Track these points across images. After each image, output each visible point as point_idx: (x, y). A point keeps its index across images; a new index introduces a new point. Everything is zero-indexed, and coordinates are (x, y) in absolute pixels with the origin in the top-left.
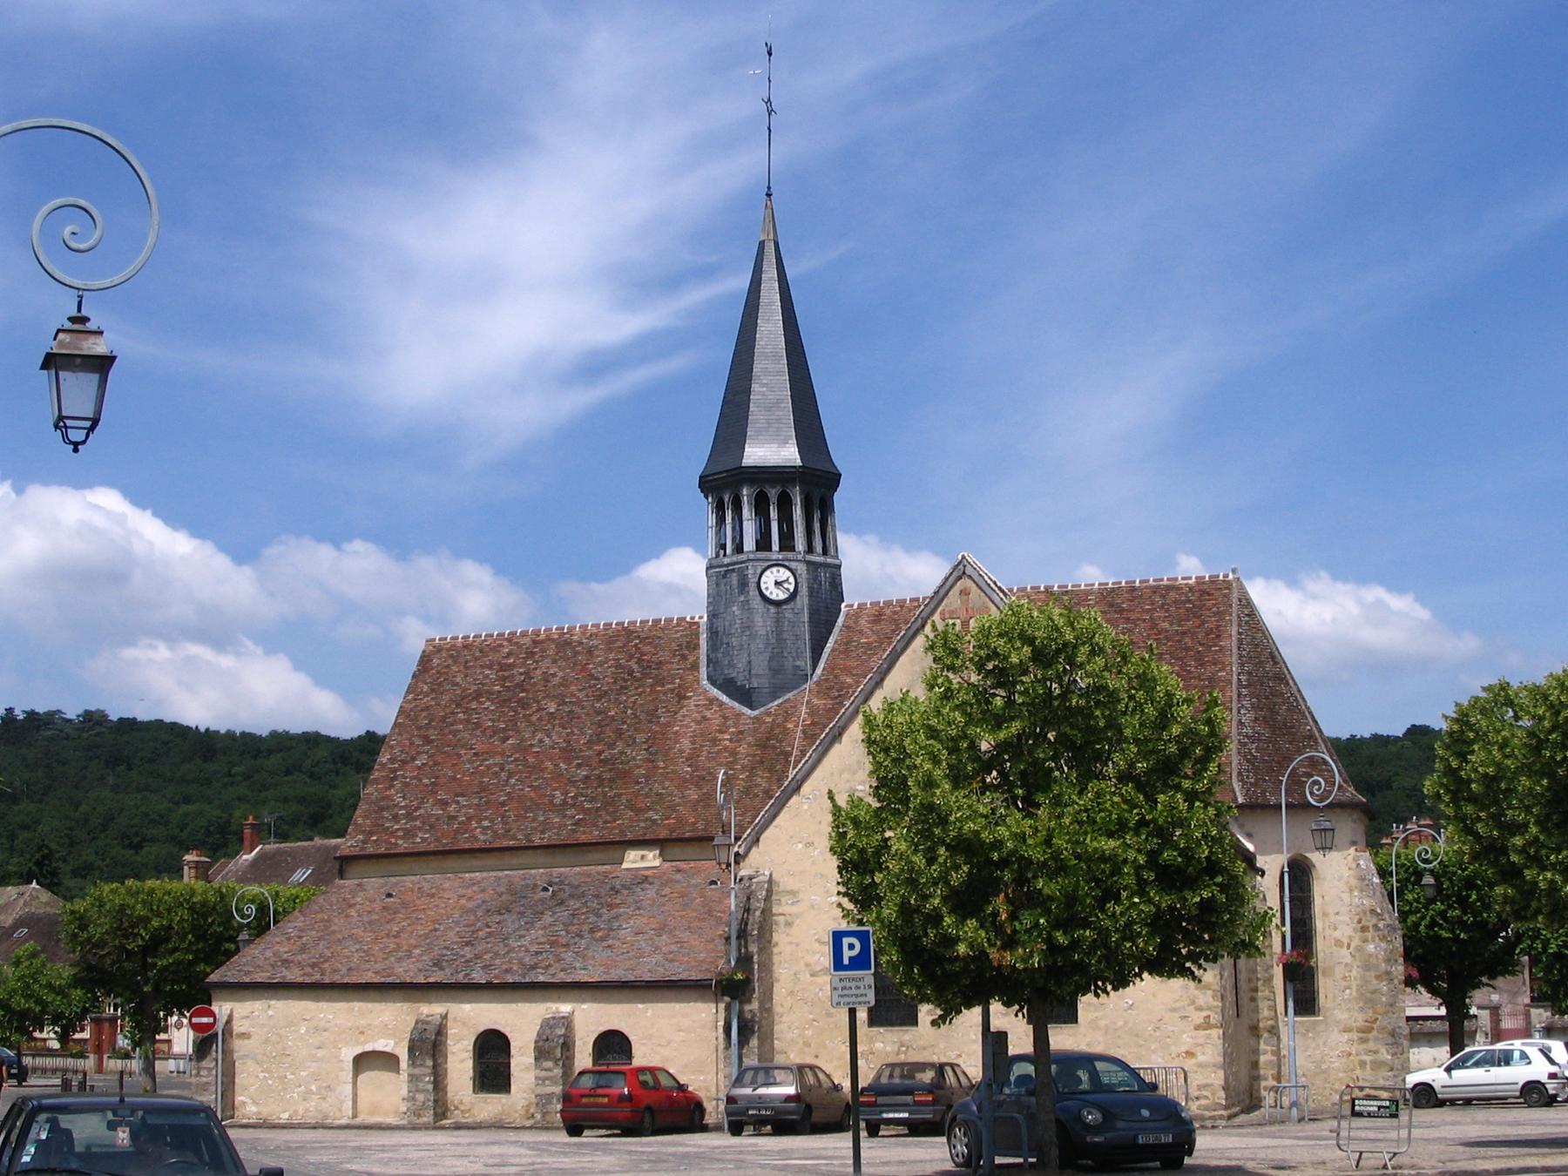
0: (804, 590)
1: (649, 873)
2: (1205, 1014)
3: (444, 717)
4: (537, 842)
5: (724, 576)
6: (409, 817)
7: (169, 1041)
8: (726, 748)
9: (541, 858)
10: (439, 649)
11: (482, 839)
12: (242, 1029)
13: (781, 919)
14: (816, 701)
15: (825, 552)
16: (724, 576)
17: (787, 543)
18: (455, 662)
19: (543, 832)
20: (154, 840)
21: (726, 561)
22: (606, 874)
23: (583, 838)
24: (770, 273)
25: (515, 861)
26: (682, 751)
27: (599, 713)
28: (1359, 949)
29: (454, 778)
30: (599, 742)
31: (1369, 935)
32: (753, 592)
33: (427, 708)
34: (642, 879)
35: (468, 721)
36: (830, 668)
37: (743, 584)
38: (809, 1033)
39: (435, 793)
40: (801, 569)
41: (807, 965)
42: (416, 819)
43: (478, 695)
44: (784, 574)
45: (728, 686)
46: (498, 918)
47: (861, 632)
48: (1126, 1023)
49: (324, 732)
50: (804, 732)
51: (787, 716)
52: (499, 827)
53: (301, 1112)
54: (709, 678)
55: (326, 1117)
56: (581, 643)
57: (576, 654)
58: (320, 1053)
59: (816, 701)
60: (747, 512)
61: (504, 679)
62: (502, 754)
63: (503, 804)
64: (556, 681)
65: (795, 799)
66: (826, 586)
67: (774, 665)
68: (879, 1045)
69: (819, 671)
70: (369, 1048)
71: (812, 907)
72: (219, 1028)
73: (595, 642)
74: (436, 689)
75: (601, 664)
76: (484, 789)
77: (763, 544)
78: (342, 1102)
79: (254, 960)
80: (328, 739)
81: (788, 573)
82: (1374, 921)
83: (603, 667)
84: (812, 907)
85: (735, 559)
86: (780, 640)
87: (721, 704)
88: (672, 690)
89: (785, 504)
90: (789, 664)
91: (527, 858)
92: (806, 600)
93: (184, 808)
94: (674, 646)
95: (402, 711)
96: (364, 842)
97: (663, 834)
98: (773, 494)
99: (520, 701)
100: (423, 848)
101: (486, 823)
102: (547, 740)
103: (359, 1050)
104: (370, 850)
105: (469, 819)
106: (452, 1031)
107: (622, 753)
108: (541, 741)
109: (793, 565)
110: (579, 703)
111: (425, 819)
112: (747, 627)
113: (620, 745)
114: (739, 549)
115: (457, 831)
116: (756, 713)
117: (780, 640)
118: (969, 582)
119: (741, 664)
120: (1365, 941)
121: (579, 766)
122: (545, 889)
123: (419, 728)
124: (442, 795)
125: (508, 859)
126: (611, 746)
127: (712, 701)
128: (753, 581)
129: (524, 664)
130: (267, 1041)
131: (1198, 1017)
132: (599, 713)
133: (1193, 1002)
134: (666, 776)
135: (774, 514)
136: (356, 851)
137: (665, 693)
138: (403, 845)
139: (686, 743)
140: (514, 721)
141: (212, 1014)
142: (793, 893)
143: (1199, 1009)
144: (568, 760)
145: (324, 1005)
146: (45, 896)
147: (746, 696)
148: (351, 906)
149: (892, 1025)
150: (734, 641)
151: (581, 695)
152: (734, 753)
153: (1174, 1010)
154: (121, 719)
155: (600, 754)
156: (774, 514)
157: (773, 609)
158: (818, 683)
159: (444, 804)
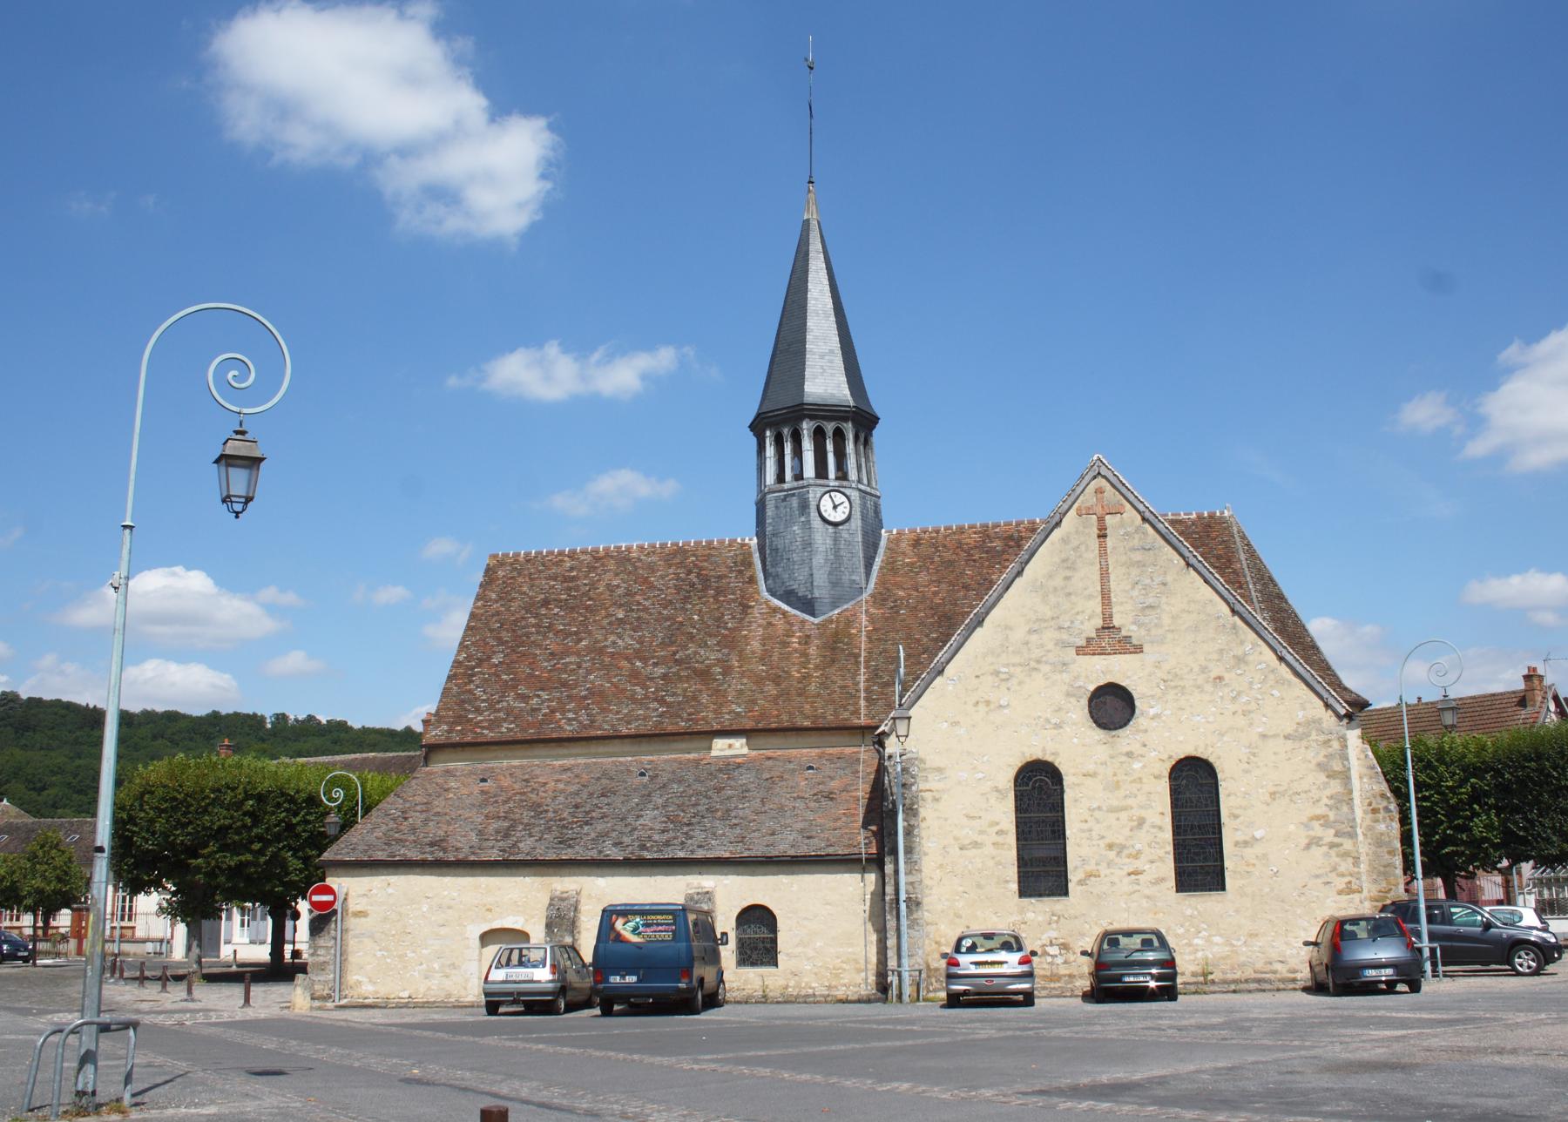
0: (857, 515)
1: (739, 760)
2: (1347, 879)
3: (516, 621)
4: (625, 731)
5: (784, 500)
6: (492, 707)
7: (133, 928)
8: (796, 650)
9: (627, 746)
10: (501, 564)
11: (569, 729)
12: (359, 908)
13: (927, 795)
14: (872, 610)
15: (869, 484)
16: (784, 500)
17: (842, 475)
18: (520, 574)
19: (629, 723)
20: (53, 785)
21: (786, 486)
22: (697, 762)
23: (670, 728)
24: (815, 246)
25: (601, 749)
26: (753, 652)
27: (667, 619)
28: (1370, 828)
29: (531, 676)
30: (672, 643)
31: (1380, 816)
32: (814, 514)
33: (498, 613)
34: (729, 766)
35: (538, 626)
36: (882, 582)
37: (804, 506)
38: (960, 904)
39: (515, 687)
40: (855, 495)
41: (956, 839)
42: (499, 710)
43: (546, 603)
44: (839, 498)
45: (789, 596)
46: (606, 801)
47: (904, 553)
48: (1272, 890)
49: (182, 710)
50: (869, 637)
51: (849, 623)
52: (583, 717)
53: (422, 990)
54: (769, 590)
55: (449, 995)
56: (639, 560)
57: (636, 568)
58: (443, 931)
59: (872, 610)
60: (808, 445)
61: (570, 589)
62: (578, 654)
63: (585, 698)
64: (620, 591)
65: (939, 679)
66: (871, 513)
67: (833, 578)
68: (1030, 916)
69: (872, 585)
70: (496, 925)
71: (959, 783)
72: (337, 906)
73: (654, 558)
74: (504, 597)
75: (662, 577)
76: (564, 684)
77: (821, 472)
78: (467, 980)
79: (363, 837)
80: (184, 717)
81: (844, 499)
82: (1385, 803)
83: (664, 579)
84: (959, 783)
85: (795, 484)
86: (837, 556)
87: (784, 613)
88: (734, 601)
89: (839, 435)
90: (846, 578)
91: (616, 747)
92: (859, 523)
93: (78, 762)
94: (730, 562)
95: (473, 616)
96: (449, 732)
97: (749, 725)
98: (829, 427)
99: (587, 608)
100: (510, 736)
101: (571, 715)
102: (620, 642)
103: (486, 928)
104: (456, 738)
105: (553, 712)
106: (583, 907)
107: (696, 653)
108: (614, 643)
109: (848, 491)
110: (646, 609)
111: (509, 711)
112: (808, 544)
113: (692, 648)
114: (799, 476)
115: (542, 722)
116: (816, 621)
117: (837, 556)
118: (1103, 482)
119: (801, 575)
120: (1377, 821)
121: (655, 665)
122: (642, 774)
123: (491, 631)
124: (522, 690)
125: (594, 748)
126: (685, 648)
127: (775, 610)
128: (813, 504)
129: (586, 577)
130: (385, 919)
131: (1340, 883)
132: (667, 619)
133: (1334, 869)
134: (743, 675)
135: (830, 447)
136: (443, 740)
137: (729, 603)
138: (490, 735)
139: (756, 645)
140: (584, 624)
141: (329, 891)
142: (939, 770)
143: (1343, 875)
144: (644, 660)
145: (447, 880)
146: (14, 810)
147: (808, 606)
148: (447, 790)
149: (1040, 895)
150: (795, 557)
151: (647, 603)
152: (805, 654)
153: (1317, 876)
154: (30, 699)
155: (675, 653)
156: (830, 447)
157: (831, 529)
158: (872, 596)
159: (524, 698)
